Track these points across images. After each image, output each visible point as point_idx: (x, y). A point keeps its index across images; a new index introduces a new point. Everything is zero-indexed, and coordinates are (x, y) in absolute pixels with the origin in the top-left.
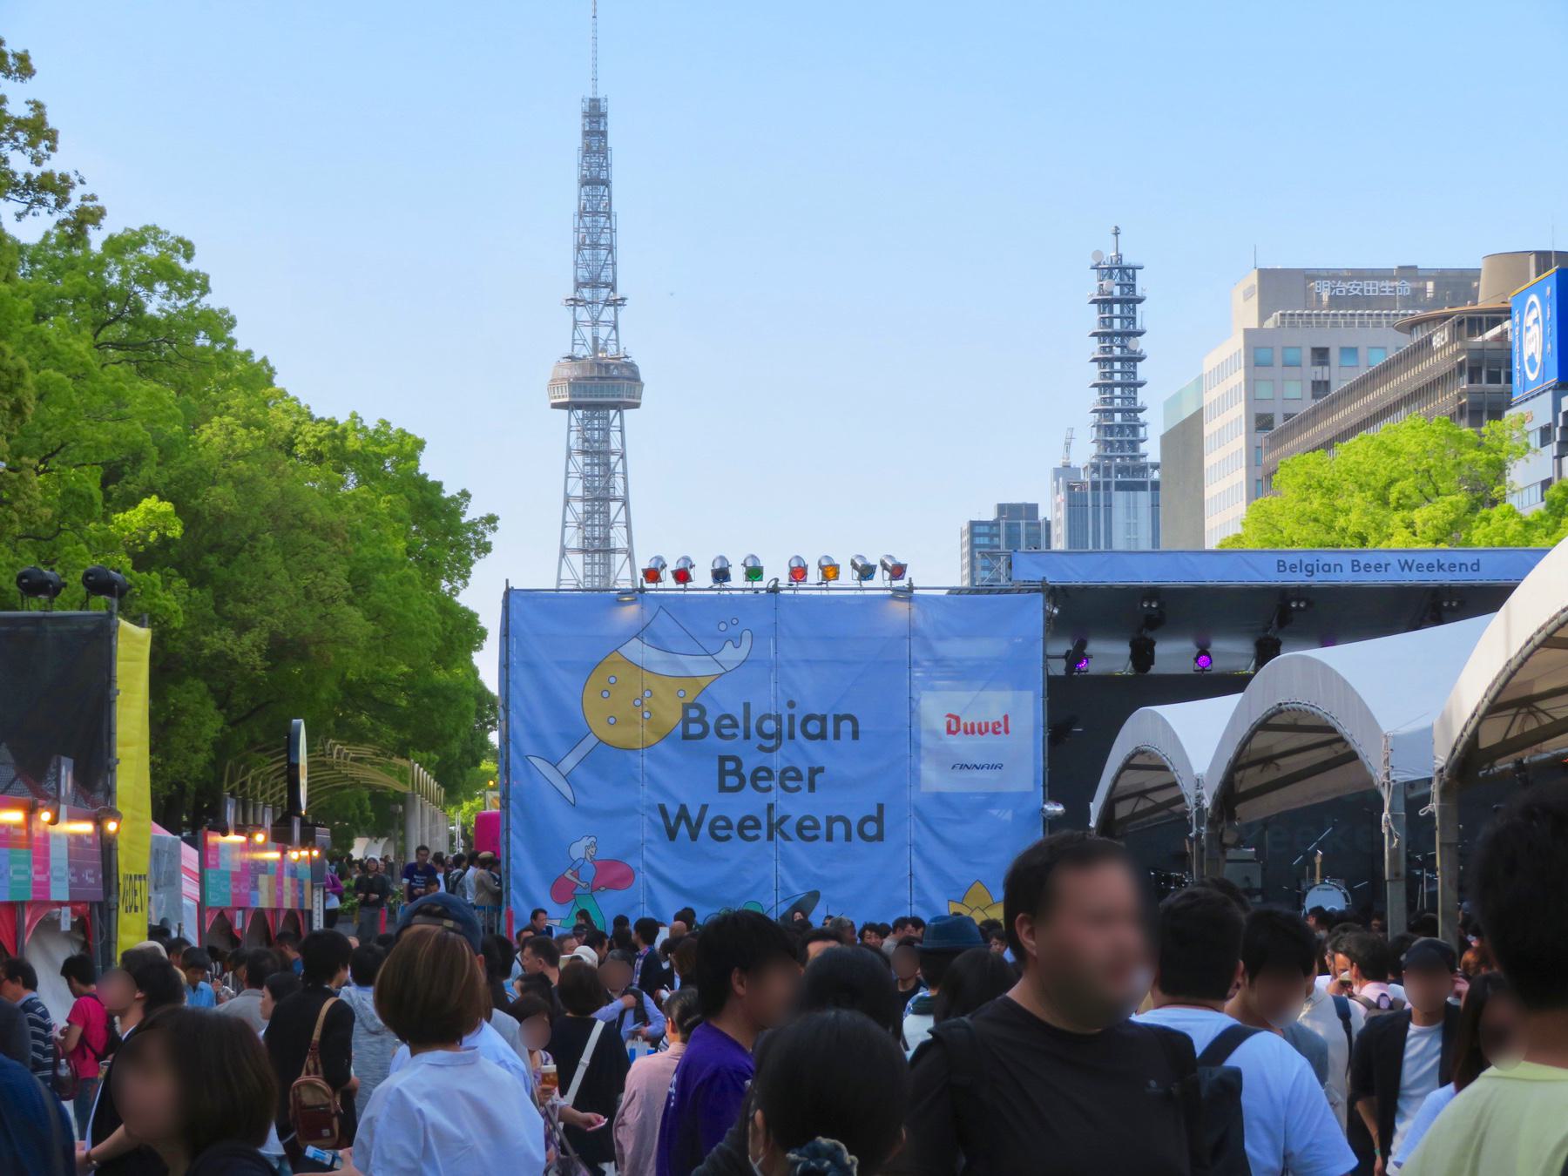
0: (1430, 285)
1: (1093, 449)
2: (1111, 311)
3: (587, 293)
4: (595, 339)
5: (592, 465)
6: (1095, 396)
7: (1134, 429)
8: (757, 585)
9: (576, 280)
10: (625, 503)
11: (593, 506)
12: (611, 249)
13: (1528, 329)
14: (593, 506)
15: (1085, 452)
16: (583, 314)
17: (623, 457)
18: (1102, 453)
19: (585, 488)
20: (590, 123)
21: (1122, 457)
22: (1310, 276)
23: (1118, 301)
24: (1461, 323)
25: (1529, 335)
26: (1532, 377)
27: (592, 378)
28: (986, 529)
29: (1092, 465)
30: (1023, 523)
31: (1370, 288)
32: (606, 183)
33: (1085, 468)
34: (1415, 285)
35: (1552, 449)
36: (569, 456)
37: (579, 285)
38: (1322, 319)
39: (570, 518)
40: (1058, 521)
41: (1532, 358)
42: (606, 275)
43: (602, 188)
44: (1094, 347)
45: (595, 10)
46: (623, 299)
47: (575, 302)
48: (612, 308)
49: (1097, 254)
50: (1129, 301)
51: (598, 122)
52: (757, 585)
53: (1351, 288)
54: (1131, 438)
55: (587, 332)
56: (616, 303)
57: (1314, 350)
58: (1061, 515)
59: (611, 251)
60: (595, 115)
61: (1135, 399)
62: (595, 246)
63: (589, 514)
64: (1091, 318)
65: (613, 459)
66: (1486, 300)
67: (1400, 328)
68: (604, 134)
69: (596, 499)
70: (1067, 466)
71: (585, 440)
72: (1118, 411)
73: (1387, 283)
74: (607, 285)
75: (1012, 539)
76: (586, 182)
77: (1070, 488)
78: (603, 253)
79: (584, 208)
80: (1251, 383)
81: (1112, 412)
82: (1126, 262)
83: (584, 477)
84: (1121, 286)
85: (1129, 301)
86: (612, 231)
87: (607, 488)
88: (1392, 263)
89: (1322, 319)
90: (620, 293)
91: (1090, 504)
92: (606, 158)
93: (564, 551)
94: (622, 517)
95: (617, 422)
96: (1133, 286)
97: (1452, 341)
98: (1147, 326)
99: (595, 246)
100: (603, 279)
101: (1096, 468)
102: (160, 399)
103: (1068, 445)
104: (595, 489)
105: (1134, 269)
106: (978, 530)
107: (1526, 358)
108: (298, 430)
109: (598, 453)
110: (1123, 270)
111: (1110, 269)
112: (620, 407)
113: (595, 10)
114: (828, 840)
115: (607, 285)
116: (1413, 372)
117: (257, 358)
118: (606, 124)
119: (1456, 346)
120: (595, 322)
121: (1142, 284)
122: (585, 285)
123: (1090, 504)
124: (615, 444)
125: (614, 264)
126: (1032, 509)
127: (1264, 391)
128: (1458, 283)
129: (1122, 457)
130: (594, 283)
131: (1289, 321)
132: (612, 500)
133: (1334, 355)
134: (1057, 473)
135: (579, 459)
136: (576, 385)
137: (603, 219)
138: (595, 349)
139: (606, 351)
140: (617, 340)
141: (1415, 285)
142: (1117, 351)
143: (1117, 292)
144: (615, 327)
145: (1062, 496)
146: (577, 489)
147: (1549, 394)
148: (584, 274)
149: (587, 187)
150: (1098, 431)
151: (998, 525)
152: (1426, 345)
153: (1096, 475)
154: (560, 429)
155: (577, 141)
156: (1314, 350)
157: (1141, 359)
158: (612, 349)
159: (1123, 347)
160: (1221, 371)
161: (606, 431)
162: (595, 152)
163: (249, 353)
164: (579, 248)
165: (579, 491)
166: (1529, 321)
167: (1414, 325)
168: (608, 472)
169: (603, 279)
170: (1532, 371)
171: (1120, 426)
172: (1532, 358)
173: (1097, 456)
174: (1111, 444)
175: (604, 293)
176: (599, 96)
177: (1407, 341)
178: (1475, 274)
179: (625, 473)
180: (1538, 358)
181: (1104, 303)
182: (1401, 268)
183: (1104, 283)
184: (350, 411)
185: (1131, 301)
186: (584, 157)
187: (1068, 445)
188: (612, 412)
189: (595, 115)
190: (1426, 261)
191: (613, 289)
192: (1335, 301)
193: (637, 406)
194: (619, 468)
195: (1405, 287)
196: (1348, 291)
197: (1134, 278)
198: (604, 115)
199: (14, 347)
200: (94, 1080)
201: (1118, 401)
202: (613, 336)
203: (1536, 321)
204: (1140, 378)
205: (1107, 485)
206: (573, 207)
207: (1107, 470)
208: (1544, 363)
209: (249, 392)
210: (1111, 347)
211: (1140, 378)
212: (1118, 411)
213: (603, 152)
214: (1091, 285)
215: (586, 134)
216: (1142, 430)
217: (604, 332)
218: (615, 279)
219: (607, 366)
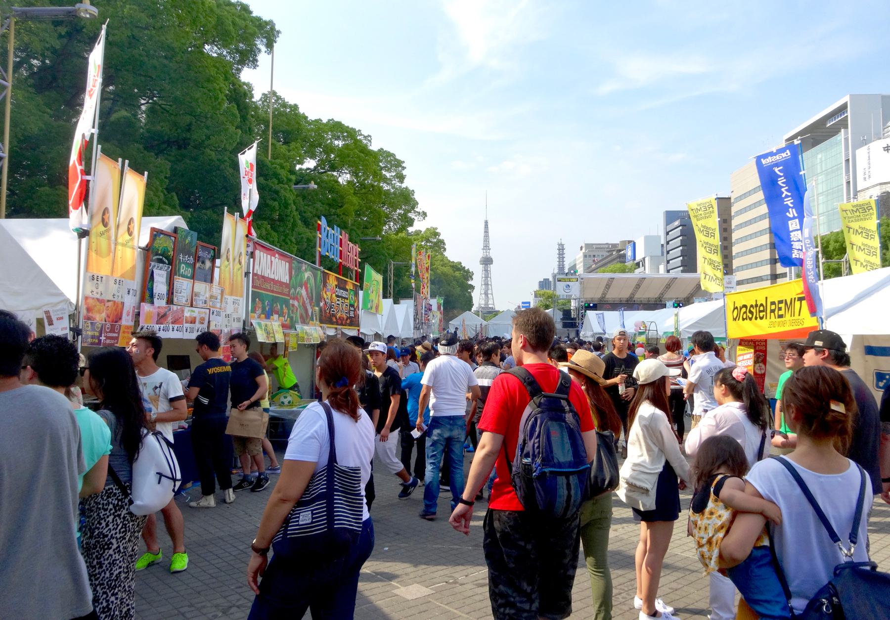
6: (558, 263)
15: (556, 271)
16: (485, 251)
31: (602, 246)
44: (558, 256)
47: (484, 249)
53: (597, 246)
56: (489, 249)
60: (486, 222)
66: (620, 248)
75: (546, 284)
76: (485, 232)
93: (481, 294)
102: (150, 194)
108: (32, 191)
117: (466, 269)
128: (614, 245)
131: (589, 251)
135: (484, 286)
136: (484, 261)
146: (484, 276)
152: (612, 254)
156: (726, 229)
160: (579, 259)
163: (464, 267)
167: (609, 251)
177: (608, 254)
178: (618, 244)
181: (559, 249)
185: (563, 249)
189: (486, 222)
192: (596, 248)
195: (607, 246)
206: (483, 231)
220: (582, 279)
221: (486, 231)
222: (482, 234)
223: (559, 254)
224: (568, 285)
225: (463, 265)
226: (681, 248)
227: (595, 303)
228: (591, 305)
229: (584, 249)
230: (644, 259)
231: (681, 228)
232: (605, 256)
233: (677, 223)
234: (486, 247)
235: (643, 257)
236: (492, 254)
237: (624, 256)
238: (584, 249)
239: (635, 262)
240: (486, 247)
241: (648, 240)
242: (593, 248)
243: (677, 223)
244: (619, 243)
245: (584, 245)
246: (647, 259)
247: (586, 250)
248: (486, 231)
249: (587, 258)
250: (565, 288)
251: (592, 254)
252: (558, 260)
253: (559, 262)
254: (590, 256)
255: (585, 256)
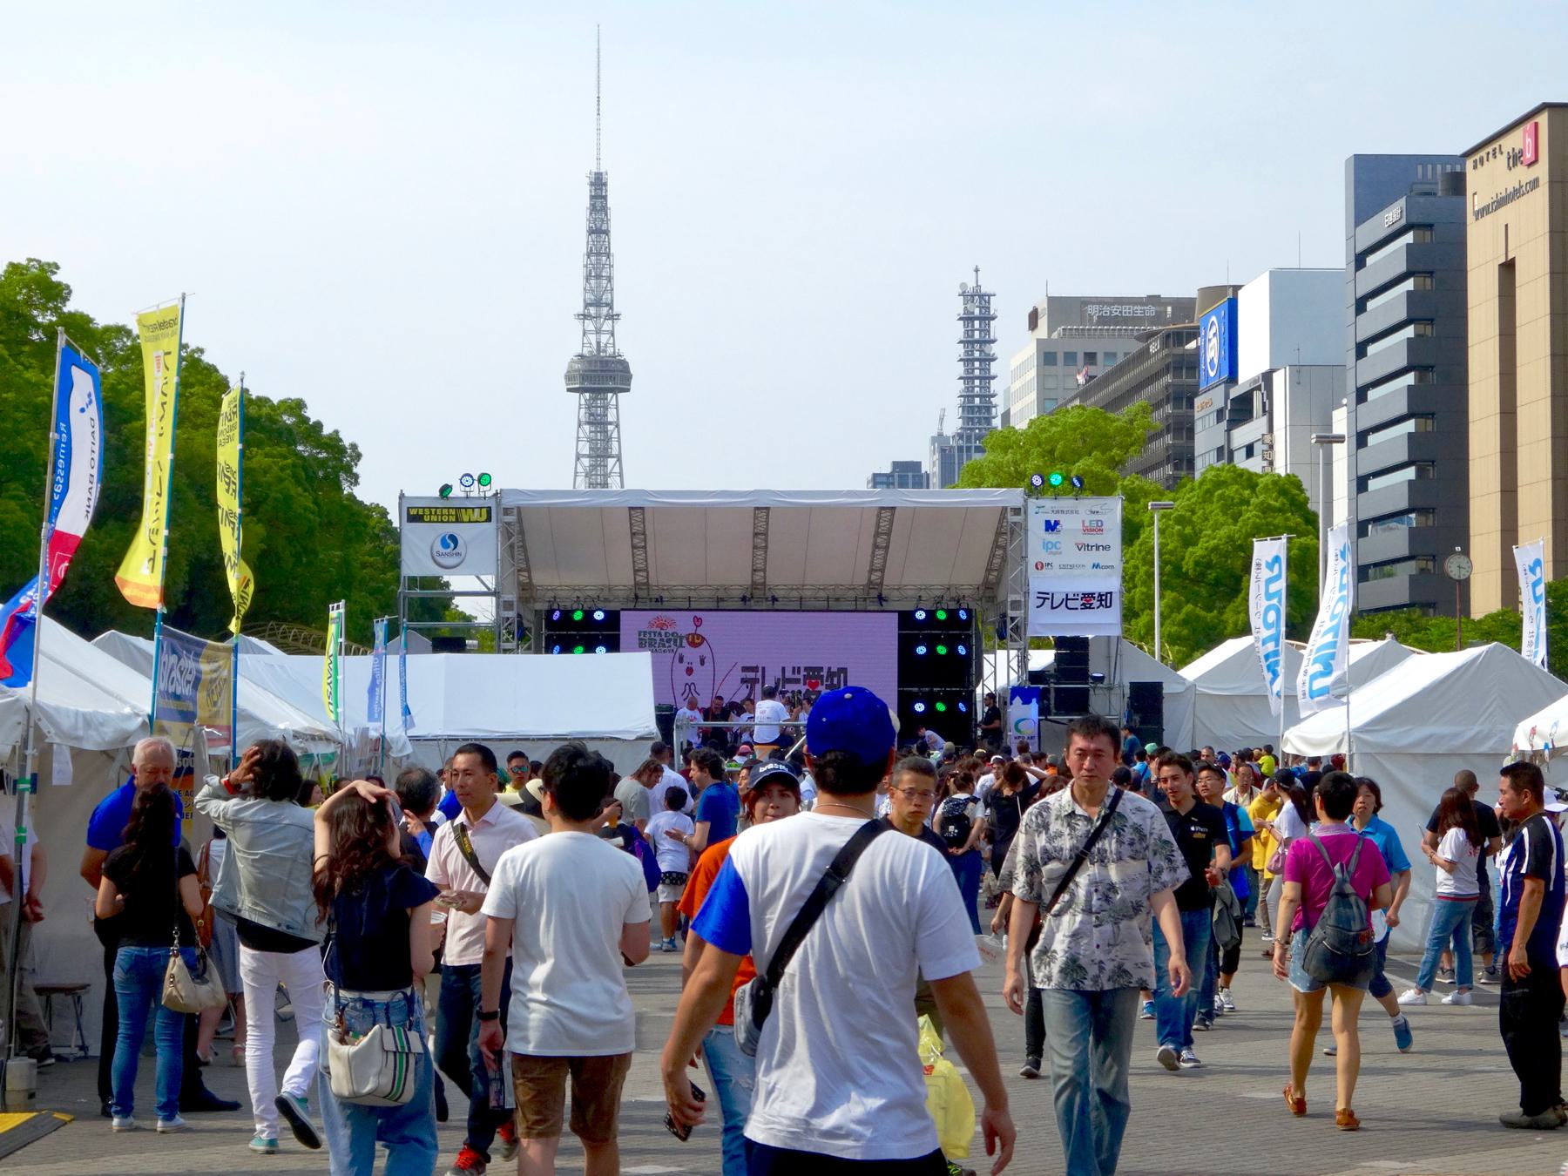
0: (1169, 309)
1: (960, 423)
2: (973, 326)
3: (592, 310)
4: (598, 343)
5: (596, 432)
7: (988, 409)
8: (1009, 607)
9: (585, 300)
10: (619, 459)
11: (596, 461)
12: (609, 279)
13: (1210, 340)
14: (596, 461)
15: (953, 425)
16: (590, 325)
17: (617, 426)
18: (966, 426)
19: (591, 449)
20: (596, 190)
21: (980, 429)
22: (1084, 302)
23: (977, 318)
24: (1168, 336)
25: (1211, 345)
26: (1212, 374)
27: (596, 371)
28: (884, 479)
29: (958, 434)
30: (910, 474)
31: (1127, 311)
32: (607, 232)
33: (953, 437)
34: (1158, 309)
35: (1224, 425)
36: (580, 426)
37: (587, 305)
38: (1092, 332)
39: (580, 469)
40: (934, 473)
41: (1212, 360)
42: (606, 298)
43: (603, 236)
44: (961, 350)
45: (599, 110)
46: (618, 315)
47: (585, 317)
48: (610, 322)
49: (963, 285)
50: (985, 319)
51: (601, 190)
52: (1009, 607)
53: (1115, 310)
54: (986, 415)
55: (593, 338)
56: (613, 317)
57: (1086, 354)
58: (937, 469)
59: (610, 281)
60: (598, 183)
61: (989, 388)
62: (598, 277)
63: (593, 467)
64: (959, 330)
65: (610, 428)
67: (1138, 338)
68: (605, 198)
69: (598, 456)
70: (940, 435)
71: (591, 415)
72: (977, 396)
73: (1139, 308)
74: (607, 305)
76: (591, 232)
77: (943, 450)
78: (604, 282)
79: (591, 250)
80: (1041, 377)
81: (973, 397)
82: (983, 290)
83: (590, 440)
84: (981, 308)
85: (985, 319)
86: (611, 266)
87: (606, 449)
88: (1142, 293)
89: (1092, 332)
90: (616, 311)
91: (956, 462)
92: (606, 215)
94: (617, 469)
95: (613, 402)
96: (989, 308)
97: (1162, 349)
98: (997, 337)
99: (598, 277)
100: (604, 301)
101: (961, 436)
103: (942, 420)
104: (598, 449)
105: (989, 296)
106: (878, 479)
107: (1208, 361)
109: (601, 423)
110: (981, 296)
111: (972, 296)
112: (615, 391)
113: (599, 110)
114: (742, 679)
115: (607, 305)
116: (1137, 370)
117: (327, 431)
118: (606, 191)
119: (1166, 351)
120: (598, 331)
121: (995, 305)
122: (591, 305)
123: (956, 462)
124: (611, 417)
125: (612, 289)
126: (918, 464)
127: (1051, 383)
129: (980, 429)
130: (598, 303)
132: (610, 457)
133: (1100, 358)
134: (934, 440)
135: (587, 428)
136: (584, 377)
137: (604, 258)
138: (599, 350)
139: (606, 352)
140: (614, 344)
141: (1158, 309)
142: (977, 354)
143: (977, 312)
144: (613, 335)
145: (937, 456)
147: (1223, 386)
148: (590, 297)
149: (593, 236)
150: (963, 411)
151: (893, 476)
153: (961, 442)
154: (573, 405)
155: (586, 202)
156: (1086, 354)
157: (994, 360)
158: (610, 350)
159: (981, 351)
161: (606, 408)
162: (598, 211)
164: (588, 278)
165: (586, 451)
166: (1210, 335)
168: (608, 439)
169: (604, 301)
170: (1212, 370)
171: (978, 407)
172: (1212, 360)
173: (961, 428)
174: (972, 419)
175: (605, 310)
176: (602, 170)
179: (619, 437)
180: (1216, 361)
181: (968, 319)
182: (1149, 297)
183: (968, 306)
184: (204, 347)
185: (987, 318)
186: (591, 214)
187: (942, 420)
188: (610, 395)
189: (598, 183)
190: (1167, 292)
191: (611, 308)
193: (628, 390)
194: (615, 435)
195: (1151, 310)
196: (1111, 312)
197: (989, 303)
198: (605, 184)
199: (1048, 846)
200: (207, 638)
201: (977, 389)
202: (611, 341)
203: (1215, 334)
204: (993, 373)
205: (969, 449)
207: (969, 437)
208: (1219, 364)
209: (1308, 568)
210: (972, 351)
211: (993, 373)
212: (977, 396)
213: (605, 209)
214: (958, 307)
215: (592, 197)
216: (994, 409)
217: (604, 338)
218: (612, 301)
219: (607, 362)
220: (507, 511)
221: (599, 230)
222: (579, 241)
223: (968, 342)
224: (453, 538)
225: (312, 414)
226: (1409, 331)
227: (613, 606)
228: (599, 616)
229: (1043, 322)
230: (1267, 377)
231: (1409, 238)
232: (1121, 359)
233: (1392, 215)
234: (599, 306)
235: (1266, 367)
236: (627, 343)
237: (1191, 364)
238: (1043, 322)
239: (1235, 392)
240: (599, 306)
241: (1285, 284)
242: (1083, 317)
243: (1392, 215)
244: (1194, 294)
245: (1043, 306)
246: (1279, 379)
247: (1051, 330)
248: (599, 230)
249: (1060, 368)
250: (438, 547)
251: (1080, 347)
252: (960, 369)
253: (968, 379)
254: (1070, 358)
255: (1047, 358)
